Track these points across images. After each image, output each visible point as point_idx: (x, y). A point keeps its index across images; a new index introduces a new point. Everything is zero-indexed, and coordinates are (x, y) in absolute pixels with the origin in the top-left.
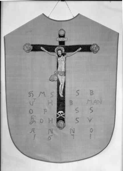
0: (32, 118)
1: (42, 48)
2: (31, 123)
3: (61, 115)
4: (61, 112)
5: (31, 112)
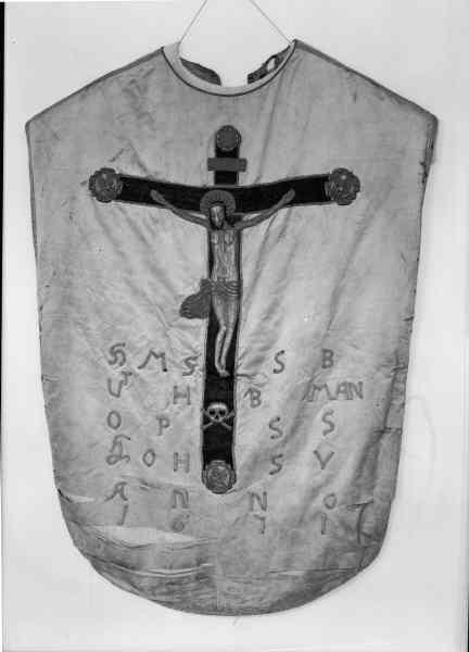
0: (115, 443)
1: (154, 193)
2: (113, 459)
3: (217, 417)
4: (217, 406)
5: (114, 420)
